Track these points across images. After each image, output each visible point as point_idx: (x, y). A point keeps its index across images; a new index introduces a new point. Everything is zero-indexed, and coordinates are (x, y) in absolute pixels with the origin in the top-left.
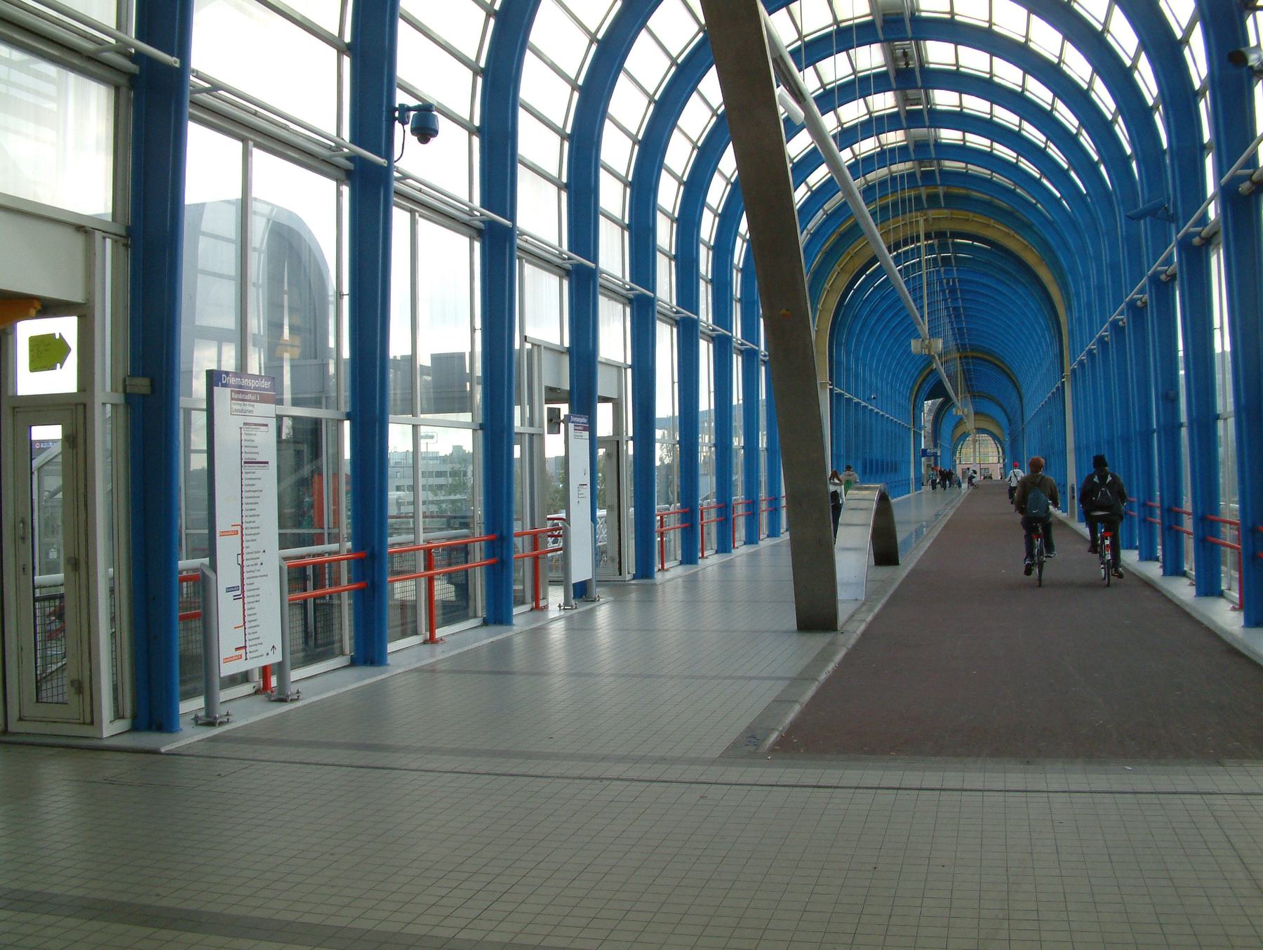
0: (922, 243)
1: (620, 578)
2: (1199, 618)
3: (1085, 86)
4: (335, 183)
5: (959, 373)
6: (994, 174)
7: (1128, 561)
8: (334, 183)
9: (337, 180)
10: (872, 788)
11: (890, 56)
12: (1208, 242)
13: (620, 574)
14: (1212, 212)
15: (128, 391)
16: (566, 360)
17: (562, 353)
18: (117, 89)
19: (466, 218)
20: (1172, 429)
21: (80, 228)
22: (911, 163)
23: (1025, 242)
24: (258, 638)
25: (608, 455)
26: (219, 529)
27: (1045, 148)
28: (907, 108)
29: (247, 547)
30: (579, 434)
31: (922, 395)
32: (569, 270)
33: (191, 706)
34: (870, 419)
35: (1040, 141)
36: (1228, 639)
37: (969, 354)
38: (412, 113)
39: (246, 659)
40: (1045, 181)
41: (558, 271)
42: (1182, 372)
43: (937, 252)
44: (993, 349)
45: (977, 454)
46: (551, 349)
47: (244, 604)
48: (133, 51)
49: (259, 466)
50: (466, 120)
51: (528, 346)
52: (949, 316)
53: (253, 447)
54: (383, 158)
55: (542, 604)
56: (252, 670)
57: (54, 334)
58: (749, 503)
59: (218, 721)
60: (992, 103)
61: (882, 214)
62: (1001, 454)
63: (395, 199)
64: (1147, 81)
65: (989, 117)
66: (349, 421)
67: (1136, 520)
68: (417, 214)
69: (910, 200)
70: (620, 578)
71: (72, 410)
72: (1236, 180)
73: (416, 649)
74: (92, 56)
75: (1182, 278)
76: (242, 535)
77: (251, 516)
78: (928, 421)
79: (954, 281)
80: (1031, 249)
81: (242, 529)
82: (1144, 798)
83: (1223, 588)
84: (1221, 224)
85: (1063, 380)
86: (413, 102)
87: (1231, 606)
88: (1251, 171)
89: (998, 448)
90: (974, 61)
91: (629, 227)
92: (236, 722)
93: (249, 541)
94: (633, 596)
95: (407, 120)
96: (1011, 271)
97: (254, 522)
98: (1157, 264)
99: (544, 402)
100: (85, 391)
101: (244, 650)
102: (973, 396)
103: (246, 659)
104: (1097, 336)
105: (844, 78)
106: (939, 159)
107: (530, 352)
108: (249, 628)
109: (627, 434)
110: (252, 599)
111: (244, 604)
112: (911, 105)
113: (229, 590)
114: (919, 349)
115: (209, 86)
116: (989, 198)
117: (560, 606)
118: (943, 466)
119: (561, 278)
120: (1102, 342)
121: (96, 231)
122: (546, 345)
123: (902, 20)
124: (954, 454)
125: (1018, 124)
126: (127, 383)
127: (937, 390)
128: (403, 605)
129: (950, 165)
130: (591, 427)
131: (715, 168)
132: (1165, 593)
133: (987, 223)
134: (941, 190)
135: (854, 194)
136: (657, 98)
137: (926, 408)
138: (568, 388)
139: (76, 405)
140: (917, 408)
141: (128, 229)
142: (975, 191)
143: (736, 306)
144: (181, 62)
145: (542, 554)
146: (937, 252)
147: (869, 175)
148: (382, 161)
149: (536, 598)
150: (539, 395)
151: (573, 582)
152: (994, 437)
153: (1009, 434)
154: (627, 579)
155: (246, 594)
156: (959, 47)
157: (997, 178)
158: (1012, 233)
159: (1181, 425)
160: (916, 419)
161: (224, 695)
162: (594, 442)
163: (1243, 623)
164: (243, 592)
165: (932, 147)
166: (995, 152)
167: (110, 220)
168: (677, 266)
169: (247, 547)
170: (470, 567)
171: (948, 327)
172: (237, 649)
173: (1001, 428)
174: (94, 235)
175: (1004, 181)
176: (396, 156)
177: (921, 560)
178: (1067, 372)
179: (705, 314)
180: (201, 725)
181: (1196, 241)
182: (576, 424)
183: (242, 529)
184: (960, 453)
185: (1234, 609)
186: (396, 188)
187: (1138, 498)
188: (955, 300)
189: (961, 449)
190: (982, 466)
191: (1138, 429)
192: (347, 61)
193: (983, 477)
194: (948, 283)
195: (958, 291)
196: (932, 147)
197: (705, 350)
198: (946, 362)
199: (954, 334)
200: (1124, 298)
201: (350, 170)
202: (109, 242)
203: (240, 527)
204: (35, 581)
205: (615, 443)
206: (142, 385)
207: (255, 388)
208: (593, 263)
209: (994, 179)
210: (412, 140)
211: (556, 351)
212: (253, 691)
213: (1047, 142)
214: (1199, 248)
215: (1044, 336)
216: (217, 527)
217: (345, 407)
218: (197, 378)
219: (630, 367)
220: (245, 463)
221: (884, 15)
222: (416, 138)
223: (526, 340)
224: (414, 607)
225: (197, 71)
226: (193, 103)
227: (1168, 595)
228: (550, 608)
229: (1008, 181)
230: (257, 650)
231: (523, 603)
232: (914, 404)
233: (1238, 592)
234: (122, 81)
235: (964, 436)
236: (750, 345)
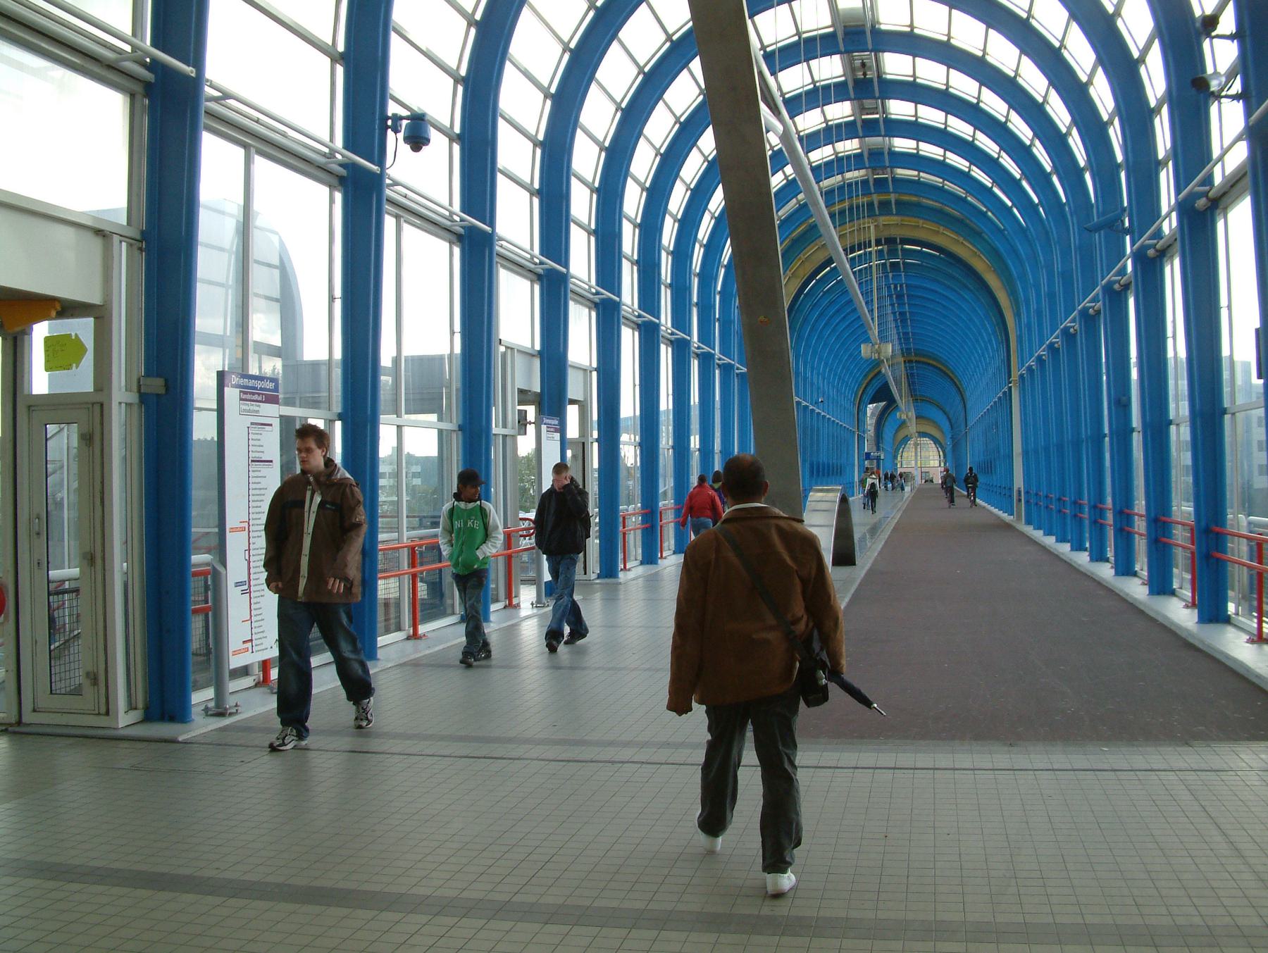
0: (873, 249)
1: (585, 577)
2: (1152, 614)
3: (1040, 100)
4: (328, 189)
5: (903, 376)
6: (946, 182)
7: (1080, 562)
8: (327, 189)
9: (330, 186)
10: (869, 768)
11: (849, 67)
12: (1163, 254)
13: (585, 574)
15: (142, 391)
17: (533, 356)
18: (132, 96)
19: (449, 223)
20: (1123, 433)
21: (99, 233)
22: (864, 170)
23: (975, 250)
24: (262, 632)
25: (574, 456)
26: (228, 526)
27: (998, 158)
28: (863, 117)
29: (254, 544)
31: (867, 398)
32: (541, 275)
33: (201, 697)
34: (818, 421)
35: (994, 151)
36: (1184, 635)
37: (914, 359)
38: (405, 122)
39: (253, 652)
40: (996, 190)
41: (529, 275)
42: (1105, 378)
43: (886, 258)
44: (939, 354)
45: (919, 458)
46: (522, 352)
47: (250, 598)
48: (148, 60)
49: (256, 465)
50: (446, 127)
52: (895, 320)
53: (259, 446)
54: (376, 166)
55: (515, 601)
56: (252, 664)
57: (70, 335)
58: (679, 509)
59: (229, 712)
60: (975, 128)
61: (839, 218)
62: (942, 458)
63: (387, 207)
64: (1103, 95)
65: (943, 126)
66: (340, 422)
67: (1086, 522)
68: (402, 220)
69: (863, 206)
70: (585, 577)
71: (88, 408)
72: (1193, 196)
73: (400, 644)
74: (111, 64)
75: (1137, 285)
76: (249, 532)
77: (257, 513)
78: (870, 425)
79: (901, 286)
80: (980, 256)
81: (249, 526)
82: (1122, 775)
83: (1174, 587)
84: (1178, 236)
85: (1010, 385)
86: (404, 113)
87: (1184, 604)
88: (1207, 188)
89: (939, 451)
90: (931, 73)
91: (595, 232)
92: (243, 713)
93: (255, 537)
94: (598, 595)
95: (399, 128)
96: (957, 276)
97: (260, 519)
98: (1112, 273)
99: (517, 404)
100: (101, 390)
101: (250, 643)
102: (915, 400)
103: (253, 652)
104: (1048, 342)
106: (892, 167)
107: (504, 355)
108: (255, 622)
109: (592, 436)
110: (258, 594)
111: (250, 598)
112: (867, 114)
113: (238, 584)
114: (869, 354)
115: (220, 94)
116: (941, 205)
117: (532, 604)
118: (886, 468)
119: (532, 282)
120: (1052, 348)
121: (115, 235)
123: (864, 32)
124: (895, 457)
125: (972, 134)
126: (141, 383)
127: (883, 394)
128: (387, 604)
129: (902, 172)
130: (562, 429)
131: (677, 175)
132: (1117, 591)
133: (937, 229)
134: (893, 197)
135: (819, 203)
136: (623, 105)
137: (869, 412)
139: (93, 404)
140: (861, 411)
141: (142, 233)
142: (927, 198)
144: (197, 73)
146: (886, 258)
148: (375, 168)
149: (509, 596)
150: (512, 397)
151: (545, 580)
152: (936, 441)
153: (951, 438)
154: (592, 579)
155: (253, 589)
156: (917, 59)
157: (949, 186)
158: (961, 239)
159: (1133, 430)
160: (860, 421)
161: (233, 686)
162: (564, 443)
163: (1196, 620)
164: (250, 586)
165: (886, 156)
166: (947, 161)
167: (125, 223)
168: (639, 271)
169: (254, 544)
170: (444, 567)
171: (894, 332)
172: (244, 642)
173: (942, 432)
174: (112, 238)
175: (953, 188)
176: (388, 165)
177: (876, 561)
178: (1015, 376)
179: (665, 319)
180: (212, 715)
181: (1151, 252)
183: (249, 526)
184: (901, 456)
185: (1187, 607)
186: (388, 196)
187: (1070, 498)
188: (901, 304)
189: (902, 452)
190: (923, 470)
191: (1089, 433)
192: (340, 70)
193: (924, 481)
194: (896, 287)
195: (906, 296)
196: (886, 156)
197: (666, 355)
198: (893, 365)
199: (899, 339)
200: (1077, 305)
201: (344, 177)
202: (124, 244)
203: (247, 524)
204: (50, 576)
206: (156, 385)
207: (261, 389)
208: (565, 268)
209: (946, 187)
210: (405, 148)
211: (530, 355)
212: (253, 684)
213: (1000, 152)
214: (1153, 260)
215: (990, 341)
216: (227, 523)
217: (337, 407)
218: (1259, 418)
219: (596, 370)
220: (252, 461)
221: (845, 27)
222: (409, 146)
223: (500, 343)
224: (398, 603)
225: (211, 81)
226: (208, 113)
227: (1121, 594)
228: (522, 605)
229: (958, 188)
230: (262, 644)
231: (497, 601)
232: (858, 407)
233: (1190, 591)
234: (138, 88)
235: (906, 439)
236: (707, 349)
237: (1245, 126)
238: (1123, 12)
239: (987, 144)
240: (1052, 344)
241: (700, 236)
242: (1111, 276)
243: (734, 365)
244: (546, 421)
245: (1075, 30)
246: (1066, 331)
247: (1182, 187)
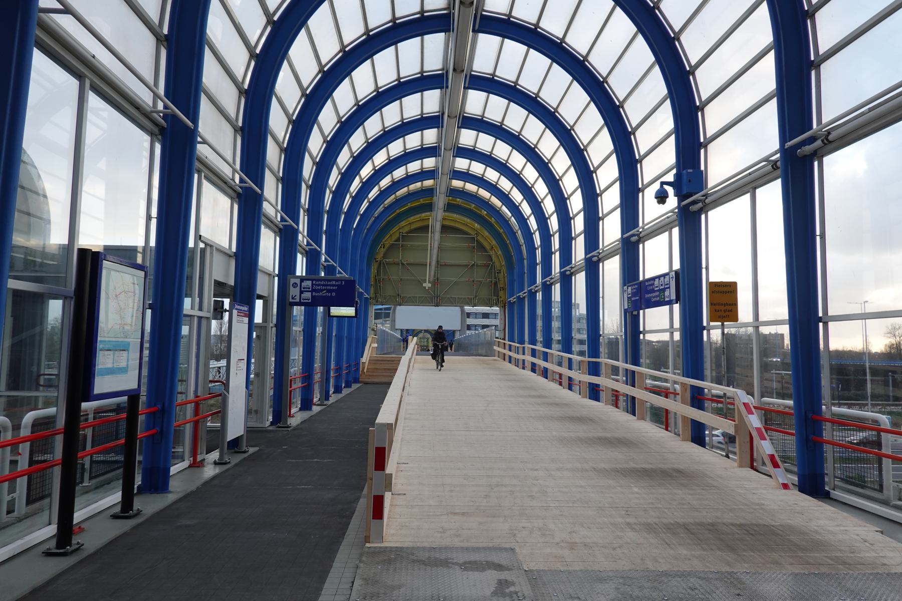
16: (233, 263)
17: (230, 256)
30: (241, 319)
32: (163, 127)
46: (220, 251)
51: (202, 245)
66: (150, 310)
107: (203, 251)
122: (218, 247)
130: (251, 315)
138: (233, 284)
145: (203, 400)
147: (494, 197)
150: (209, 289)
159: (524, 259)
182: (239, 311)
205: (262, 328)
241: (370, 195)
243: (336, 267)
244: (237, 307)
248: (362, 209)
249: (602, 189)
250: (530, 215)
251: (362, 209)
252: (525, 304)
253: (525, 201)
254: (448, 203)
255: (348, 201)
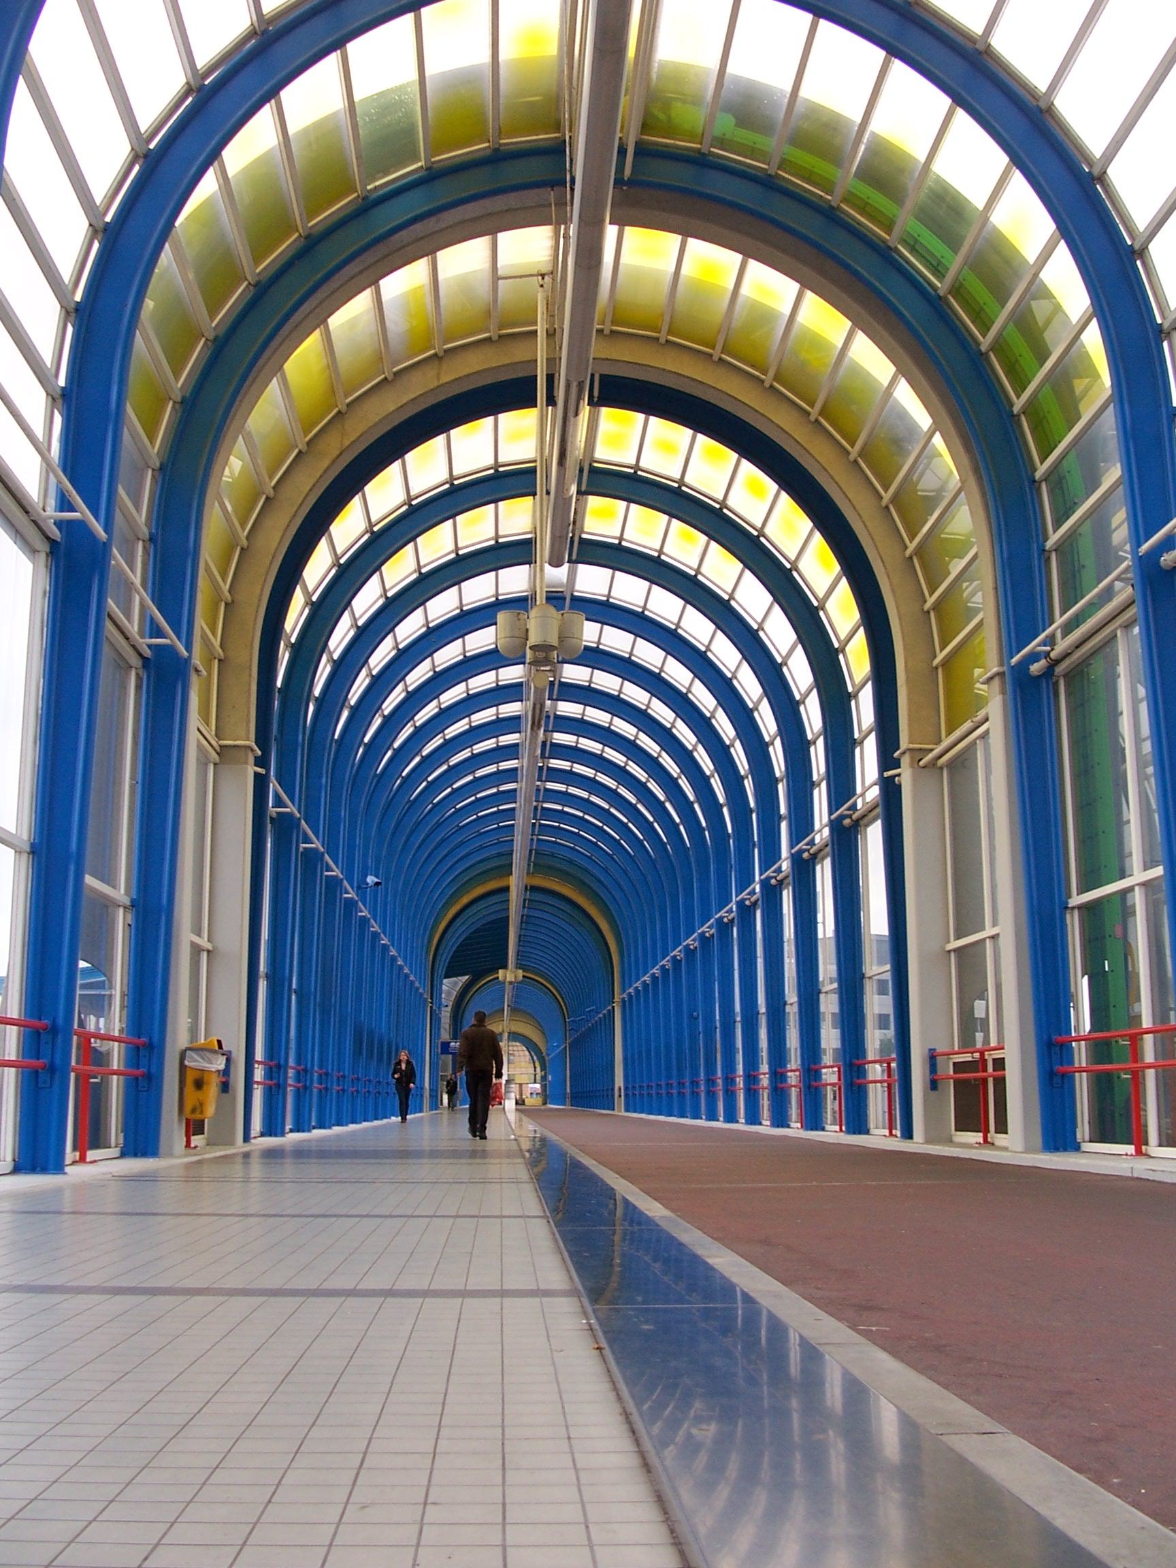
14: (785, 865)
35: (753, 619)
40: (696, 806)
89: (534, 1062)
105: (718, 587)
143: (325, 666)
237: (879, 778)
238: (807, 701)
239: (703, 758)
240: (663, 966)
242: (722, 913)
245: (800, 653)
246: (653, 975)
247: (833, 809)
248: (389, 705)
249: (803, 692)
250: (715, 709)
251: (389, 705)
252: (733, 951)
253: (697, 681)
254: (639, 145)
255: (361, 682)
